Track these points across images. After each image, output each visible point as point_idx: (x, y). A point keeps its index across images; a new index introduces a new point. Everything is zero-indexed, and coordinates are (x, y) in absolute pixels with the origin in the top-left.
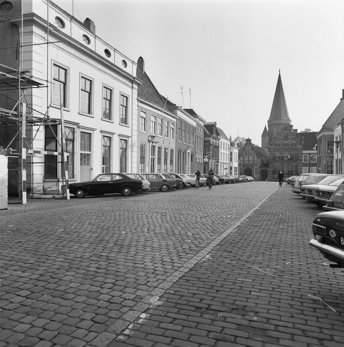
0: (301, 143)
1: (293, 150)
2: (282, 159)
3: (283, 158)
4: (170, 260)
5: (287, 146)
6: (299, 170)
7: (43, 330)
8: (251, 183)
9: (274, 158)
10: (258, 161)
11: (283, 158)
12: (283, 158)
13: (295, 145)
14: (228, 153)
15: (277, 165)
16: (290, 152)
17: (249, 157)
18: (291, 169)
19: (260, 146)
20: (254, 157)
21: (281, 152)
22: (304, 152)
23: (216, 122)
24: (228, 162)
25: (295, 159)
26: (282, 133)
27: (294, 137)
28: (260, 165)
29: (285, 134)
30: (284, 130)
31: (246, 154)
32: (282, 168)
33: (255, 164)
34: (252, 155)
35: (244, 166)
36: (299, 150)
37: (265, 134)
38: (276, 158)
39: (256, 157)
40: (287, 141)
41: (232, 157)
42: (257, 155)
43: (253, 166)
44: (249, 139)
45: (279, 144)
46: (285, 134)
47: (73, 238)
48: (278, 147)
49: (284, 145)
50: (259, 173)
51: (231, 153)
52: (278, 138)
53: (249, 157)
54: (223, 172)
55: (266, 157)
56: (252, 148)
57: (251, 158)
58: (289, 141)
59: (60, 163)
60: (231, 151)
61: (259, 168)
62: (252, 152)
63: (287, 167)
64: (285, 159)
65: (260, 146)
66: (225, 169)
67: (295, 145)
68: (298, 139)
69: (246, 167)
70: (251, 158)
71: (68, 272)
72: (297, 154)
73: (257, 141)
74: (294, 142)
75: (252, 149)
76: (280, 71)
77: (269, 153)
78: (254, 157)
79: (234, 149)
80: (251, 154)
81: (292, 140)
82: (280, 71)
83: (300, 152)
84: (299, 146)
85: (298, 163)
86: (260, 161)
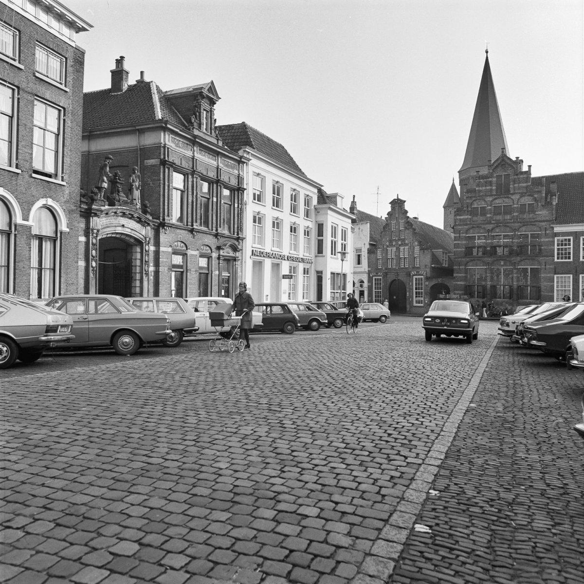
0: (548, 204)
1: (525, 223)
2: (491, 252)
3: (496, 252)
4: (289, 451)
5: (506, 213)
6: (544, 284)
7: (47, 577)
8: (383, 325)
9: (469, 251)
10: (424, 261)
11: (494, 248)
12: (494, 248)
13: (532, 209)
14: (311, 224)
15: (478, 269)
16: (515, 230)
17: (398, 249)
18: (518, 281)
19: (442, 228)
20: (412, 249)
21: (488, 231)
22: (558, 229)
23: (212, 82)
24: (311, 254)
25: (528, 251)
26: (491, 175)
27: (527, 187)
28: (428, 270)
29: (499, 177)
30: (497, 167)
31: (391, 241)
32: (492, 278)
33: (414, 268)
34: (407, 245)
35: (385, 275)
36: (543, 224)
37: (453, 204)
38: (475, 251)
39: (417, 249)
40: (506, 200)
41: (324, 238)
42: (420, 242)
43: (409, 275)
44: (398, 199)
45: (483, 208)
46: (499, 177)
47: (81, 415)
48: (479, 219)
49: (497, 211)
50: (426, 294)
51: (320, 228)
52: (480, 191)
53: (398, 249)
54: (274, 289)
55: (446, 251)
56: (408, 222)
57: (404, 252)
58: (513, 197)
59: (32, 266)
60: (321, 219)
61: (427, 279)
62: (408, 235)
63: (506, 275)
64: (499, 251)
65: (442, 228)
66: (284, 277)
67: (532, 209)
68: (540, 192)
69: (391, 277)
70: (404, 252)
71: (83, 477)
72: (538, 236)
73: (430, 212)
74: (527, 200)
75: (406, 228)
76: (487, 52)
77: (453, 235)
78: (412, 249)
79: (329, 212)
80: (403, 240)
81: (522, 195)
82: (487, 52)
83: (546, 229)
84: (543, 213)
85: (540, 264)
86: (427, 259)
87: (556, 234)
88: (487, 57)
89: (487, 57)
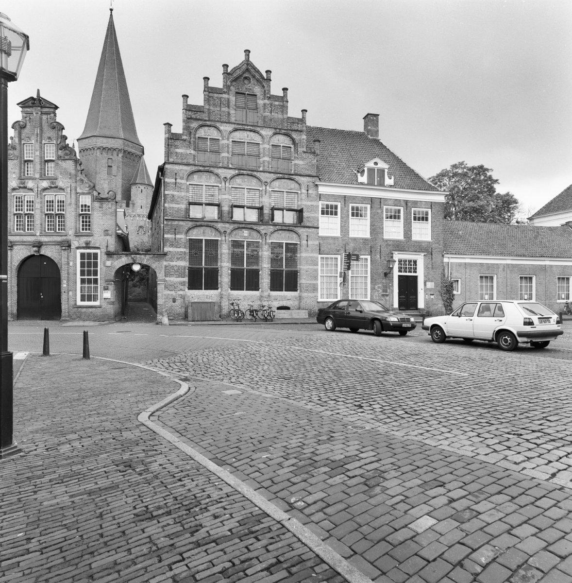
76: (111, 10)
82: (111, 10)
87: (320, 197)
88: (111, 15)
89: (111, 15)
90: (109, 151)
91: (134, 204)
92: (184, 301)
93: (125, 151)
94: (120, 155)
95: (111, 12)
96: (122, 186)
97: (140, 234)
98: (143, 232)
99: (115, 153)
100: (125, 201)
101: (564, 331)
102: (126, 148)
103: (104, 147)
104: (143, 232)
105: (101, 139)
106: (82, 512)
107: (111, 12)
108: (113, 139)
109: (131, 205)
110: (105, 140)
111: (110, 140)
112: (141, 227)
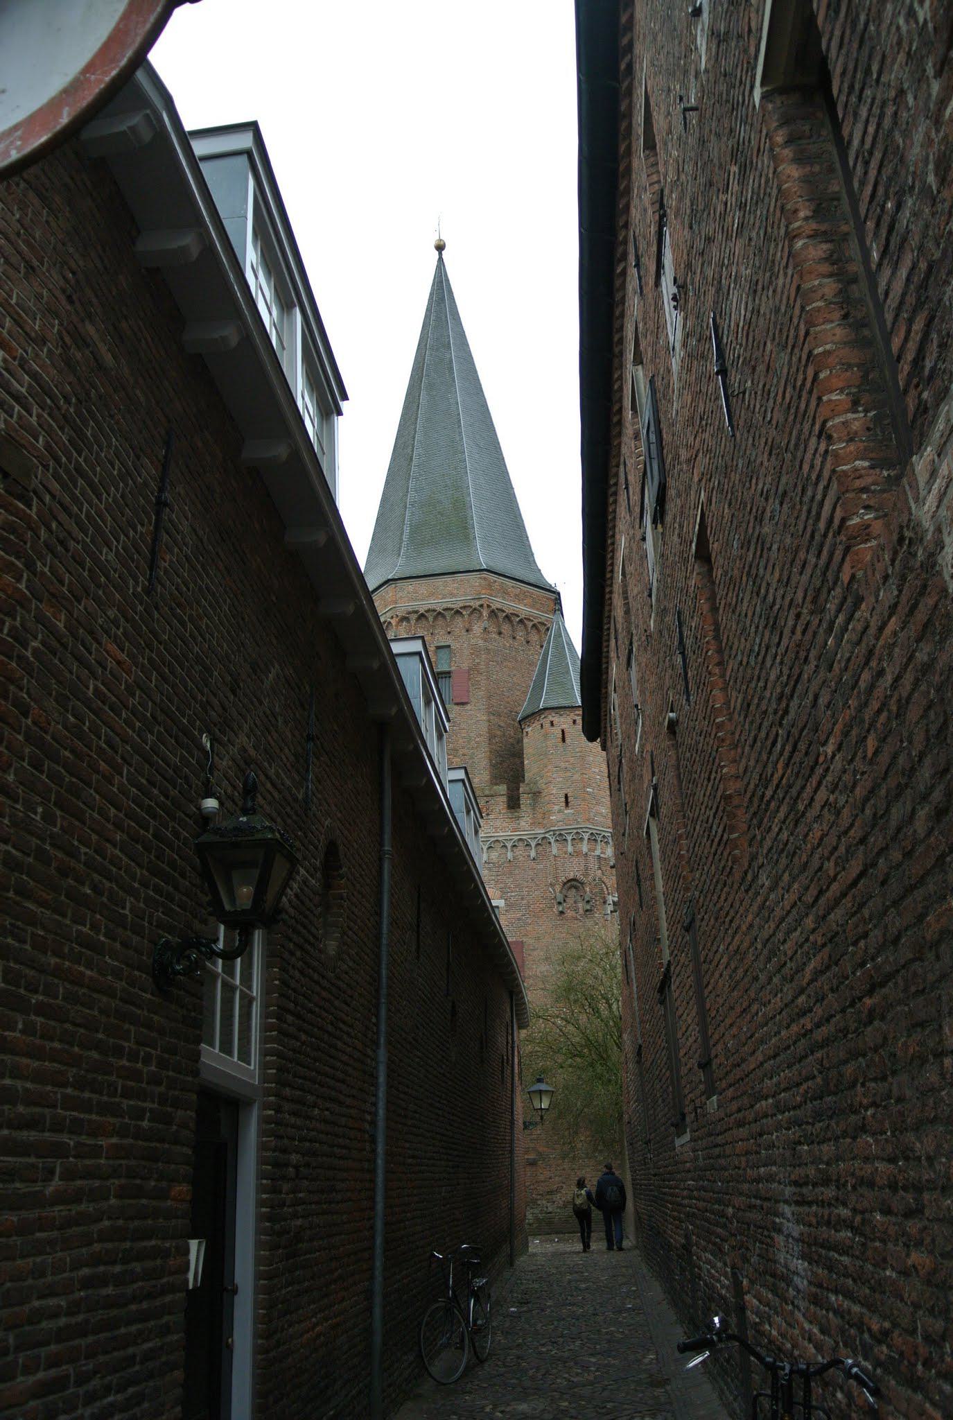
76: (440, 248)
82: (440, 248)
88: (441, 260)
89: (441, 260)
90: (440, 621)
91: (536, 794)
92: (834, 303)
93: (493, 614)
94: (477, 628)
95: (440, 254)
96: (492, 737)
97: (570, 913)
98: (581, 906)
99: (459, 623)
100: (502, 788)
101: (677, 1354)
102: (498, 602)
103: (422, 611)
104: (581, 906)
105: (409, 586)
106: (874, 204)
107: (440, 254)
108: (448, 579)
109: (525, 800)
110: (423, 587)
111: (439, 582)
112: (573, 884)
